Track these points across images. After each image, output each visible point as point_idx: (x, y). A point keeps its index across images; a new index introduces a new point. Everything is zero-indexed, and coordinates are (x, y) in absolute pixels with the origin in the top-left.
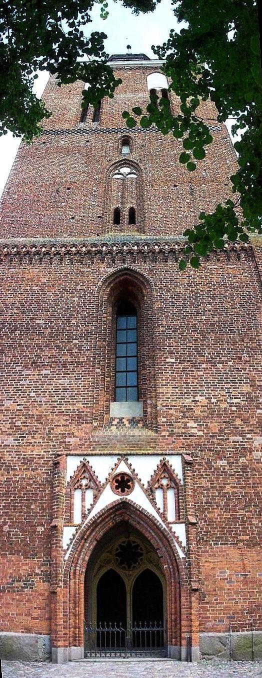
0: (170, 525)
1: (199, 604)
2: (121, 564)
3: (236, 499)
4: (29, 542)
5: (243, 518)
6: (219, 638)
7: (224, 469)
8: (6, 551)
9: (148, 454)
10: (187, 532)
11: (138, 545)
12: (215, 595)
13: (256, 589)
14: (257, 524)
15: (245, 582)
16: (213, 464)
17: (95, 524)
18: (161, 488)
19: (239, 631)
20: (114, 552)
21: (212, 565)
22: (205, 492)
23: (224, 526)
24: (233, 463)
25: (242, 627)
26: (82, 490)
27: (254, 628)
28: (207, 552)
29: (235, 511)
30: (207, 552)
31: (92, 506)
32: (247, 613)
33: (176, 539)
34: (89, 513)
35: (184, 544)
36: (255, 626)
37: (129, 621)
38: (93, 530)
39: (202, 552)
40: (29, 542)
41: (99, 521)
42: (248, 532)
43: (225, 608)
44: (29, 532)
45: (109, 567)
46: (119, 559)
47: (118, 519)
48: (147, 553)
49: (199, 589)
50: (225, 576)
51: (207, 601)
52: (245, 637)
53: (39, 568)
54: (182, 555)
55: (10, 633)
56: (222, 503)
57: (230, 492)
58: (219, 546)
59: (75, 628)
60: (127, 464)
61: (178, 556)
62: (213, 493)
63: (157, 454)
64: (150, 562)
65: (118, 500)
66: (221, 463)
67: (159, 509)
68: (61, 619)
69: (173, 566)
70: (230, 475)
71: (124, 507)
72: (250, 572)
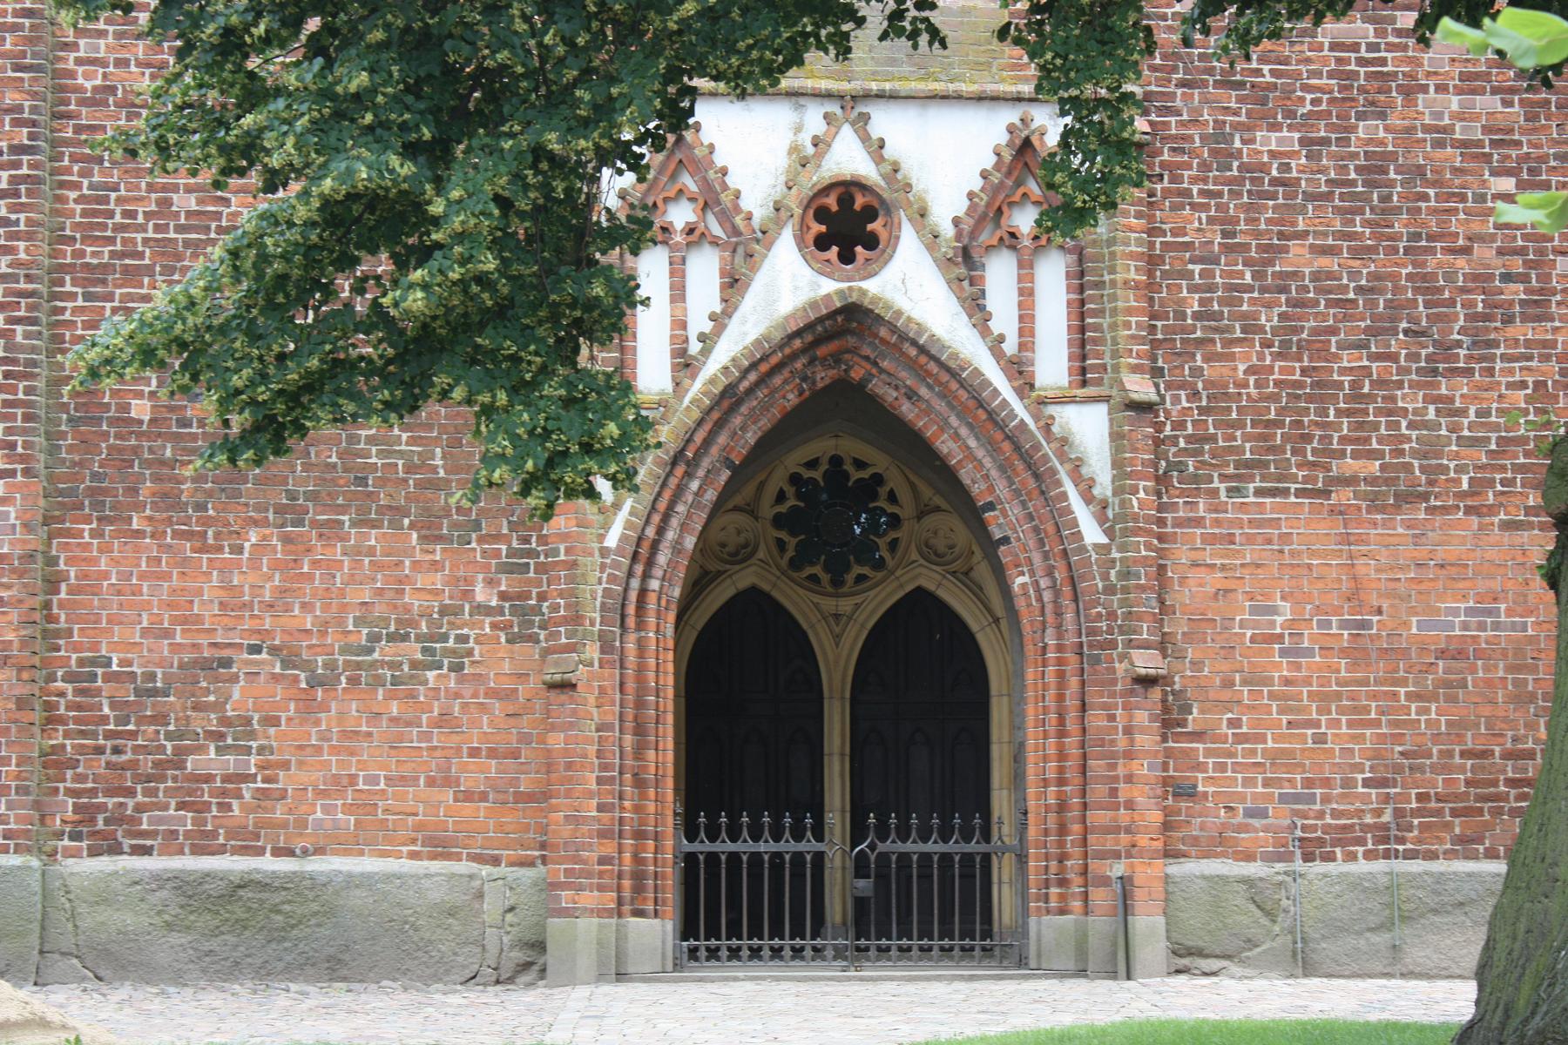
0: (1052, 410)
1: (1164, 739)
2: (795, 564)
3: (1330, 304)
4: (442, 473)
5: (1355, 385)
6: (1248, 882)
7: (1285, 168)
8: (343, 510)
9: (959, 97)
10: (1116, 437)
11: (878, 479)
12: (1227, 705)
13: (1403, 682)
14: (1416, 412)
15: (1356, 654)
16: (1237, 144)
17: (728, 399)
18: (1013, 248)
19: (1334, 860)
20: (768, 510)
21: (1214, 580)
22: (1197, 268)
23: (1272, 416)
24: (1325, 142)
25: (1345, 839)
26: (673, 249)
27: (1401, 848)
28: (1198, 522)
29: (1322, 352)
30: (1198, 522)
31: (720, 321)
32: (1367, 783)
33: (1069, 466)
34: (706, 352)
35: (1104, 483)
36: (1402, 841)
37: (836, 817)
38: (720, 424)
39: (1179, 523)
40: (442, 473)
41: (745, 384)
42: (1375, 445)
43: (1273, 755)
44: (443, 429)
45: (745, 578)
46: (792, 542)
47: (823, 377)
48: (920, 516)
49: (1164, 677)
50: (1272, 624)
51: (1198, 729)
52: (1357, 884)
53: (490, 582)
54: (1092, 533)
55: (357, 860)
56: (1268, 320)
57: (1307, 271)
58: (1252, 499)
59: (639, 835)
60: (865, 138)
61: (1078, 536)
62: (1231, 274)
63: (995, 99)
64: (933, 555)
65: (828, 296)
66: (1267, 141)
67: (1001, 339)
68: (590, 794)
69: (1054, 580)
70: (1310, 197)
71: (845, 327)
72: (1379, 612)
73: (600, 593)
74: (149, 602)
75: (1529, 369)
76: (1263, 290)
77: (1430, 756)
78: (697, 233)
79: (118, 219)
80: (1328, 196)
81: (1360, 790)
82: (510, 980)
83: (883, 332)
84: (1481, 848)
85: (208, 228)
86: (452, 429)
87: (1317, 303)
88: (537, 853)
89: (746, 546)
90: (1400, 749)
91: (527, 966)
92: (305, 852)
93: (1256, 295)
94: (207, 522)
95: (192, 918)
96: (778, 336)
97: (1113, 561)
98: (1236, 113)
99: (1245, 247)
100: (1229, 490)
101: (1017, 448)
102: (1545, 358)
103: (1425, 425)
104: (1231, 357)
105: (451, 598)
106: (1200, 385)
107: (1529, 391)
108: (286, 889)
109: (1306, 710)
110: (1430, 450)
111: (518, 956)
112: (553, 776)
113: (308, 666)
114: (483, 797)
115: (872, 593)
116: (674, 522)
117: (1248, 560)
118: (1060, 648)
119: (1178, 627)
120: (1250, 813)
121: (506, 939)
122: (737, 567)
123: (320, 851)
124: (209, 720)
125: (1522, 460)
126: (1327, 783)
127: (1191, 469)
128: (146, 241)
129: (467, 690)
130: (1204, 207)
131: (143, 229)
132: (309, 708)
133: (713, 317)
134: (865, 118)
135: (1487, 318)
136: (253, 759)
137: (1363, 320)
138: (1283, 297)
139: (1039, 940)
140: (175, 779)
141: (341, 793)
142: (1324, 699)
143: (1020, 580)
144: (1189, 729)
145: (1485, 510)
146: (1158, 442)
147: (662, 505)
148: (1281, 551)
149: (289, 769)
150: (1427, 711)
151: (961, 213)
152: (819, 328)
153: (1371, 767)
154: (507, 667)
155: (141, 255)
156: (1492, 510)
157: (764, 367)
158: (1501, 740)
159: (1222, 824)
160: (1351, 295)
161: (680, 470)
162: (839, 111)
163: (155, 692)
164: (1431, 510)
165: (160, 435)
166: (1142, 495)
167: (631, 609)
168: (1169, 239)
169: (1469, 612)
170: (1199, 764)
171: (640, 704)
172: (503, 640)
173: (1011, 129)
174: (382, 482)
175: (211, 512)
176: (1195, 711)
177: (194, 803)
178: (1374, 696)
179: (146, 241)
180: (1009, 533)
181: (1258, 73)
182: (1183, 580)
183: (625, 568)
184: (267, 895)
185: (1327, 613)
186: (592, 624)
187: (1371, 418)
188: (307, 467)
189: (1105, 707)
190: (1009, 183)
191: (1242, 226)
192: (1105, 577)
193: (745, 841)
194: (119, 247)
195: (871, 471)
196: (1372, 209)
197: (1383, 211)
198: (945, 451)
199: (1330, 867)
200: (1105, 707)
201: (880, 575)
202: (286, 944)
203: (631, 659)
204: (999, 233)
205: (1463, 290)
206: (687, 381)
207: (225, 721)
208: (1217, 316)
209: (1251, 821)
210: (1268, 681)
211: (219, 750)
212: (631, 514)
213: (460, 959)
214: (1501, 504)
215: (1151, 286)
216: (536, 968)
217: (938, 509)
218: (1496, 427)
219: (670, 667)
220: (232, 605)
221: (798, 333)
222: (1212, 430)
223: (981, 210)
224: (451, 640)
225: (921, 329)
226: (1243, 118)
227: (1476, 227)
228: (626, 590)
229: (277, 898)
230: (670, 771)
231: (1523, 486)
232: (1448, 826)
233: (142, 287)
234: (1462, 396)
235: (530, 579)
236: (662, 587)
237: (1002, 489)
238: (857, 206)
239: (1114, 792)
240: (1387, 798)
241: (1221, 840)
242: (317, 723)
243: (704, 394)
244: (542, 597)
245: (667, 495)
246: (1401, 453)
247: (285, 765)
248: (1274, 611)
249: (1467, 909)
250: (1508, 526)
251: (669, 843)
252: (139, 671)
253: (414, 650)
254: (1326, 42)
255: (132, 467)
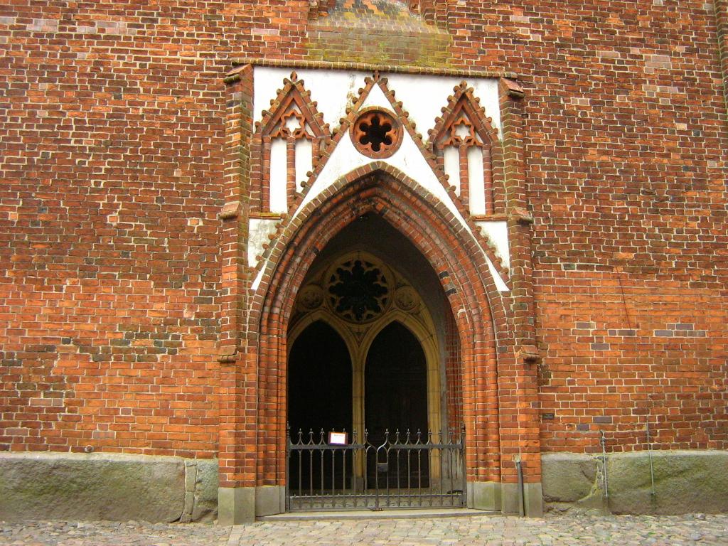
0: (479, 224)
2: (340, 310)
4: (168, 251)
5: (622, 217)
6: (581, 464)
8: (114, 269)
14: (650, 230)
16: (562, 102)
17: (316, 215)
19: (621, 451)
20: (327, 285)
27: (652, 444)
28: (551, 282)
29: (606, 200)
30: (551, 282)
31: (312, 176)
32: (635, 412)
34: (306, 191)
35: (506, 263)
36: (652, 440)
38: (310, 230)
39: (541, 282)
40: (168, 251)
43: (590, 398)
47: (363, 208)
48: (397, 288)
52: (633, 462)
53: (191, 308)
54: (501, 286)
55: (117, 454)
56: (581, 185)
58: (576, 270)
60: (385, 89)
61: (494, 287)
62: (562, 162)
64: (403, 306)
65: (367, 165)
66: (577, 101)
67: (454, 188)
72: (638, 327)
73: (249, 313)
74: (12, 316)
75: (698, 211)
76: (577, 170)
77: (664, 398)
78: (301, 134)
79: (8, 121)
80: (604, 128)
81: (632, 415)
82: (199, 520)
83: (395, 185)
84: (689, 443)
85: (54, 126)
86: (173, 229)
87: (602, 177)
88: (214, 451)
89: (317, 300)
90: (650, 394)
91: (207, 512)
92: (90, 451)
93: (574, 172)
94: (44, 274)
95: (28, 485)
96: (342, 185)
97: (512, 300)
98: (561, 88)
99: (567, 150)
100: (565, 266)
101: (462, 242)
102: (705, 207)
103: (654, 236)
104: (564, 201)
105: (170, 316)
106: (549, 214)
107: (699, 222)
108: (78, 470)
109: (604, 375)
110: (657, 248)
111: (202, 507)
112: (223, 410)
113: (94, 351)
114: (186, 421)
115: (375, 323)
116: (287, 278)
117: (575, 301)
118: (483, 345)
119: (543, 334)
120: (580, 428)
121: (196, 498)
122: (314, 310)
123: (97, 449)
124: (41, 379)
125: (698, 254)
126: (616, 412)
127: (547, 255)
128: (21, 133)
129: (178, 365)
130: (548, 131)
131: (21, 126)
132: (94, 373)
133: (309, 175)
134: (385, 82)
135: (678, 187)
136: (63, 400)
137: (624, 186)
138: (586, 174)
139: (473, 494)
140: (22, 410)
141: (110, 418)
142: (615, 371)
143: (461, 311)
144: (550, 385)
145: (683, 277)
146: (532, 242)
147: (281, 269)
148: (591, 296)
149: (82, 406)
150: (662, 376)
151: (432, 128)
152: (362, 182)
153: (637, 404)
154: (199, 352)
155: (18, 139)
156: (686, 278)
157: (334, 201)
158: (696, 390)
159: (568, 433)
160: (618, 174)
161: (291, 251)
162: (372, 79)
163: (13, 363)
164: (659, 277)
165: (22, 229)
166: (525, 266)
167: (265, 323)
168: (532, 144)
169: (678, 327)
170: (555, 403)
171: (268, 373)
172: (197, 338)
173: (455, 90)
174: (136, 255)
175: (47, 269)
176: (552, 376)
177: (31, 422)
178: (637, 368)
179: (21, 133)
180: (455, 287)
181: (570, 70)
182: (544, 310)
183: (262, 301)
184: (69, 473)
185: (613, 327)
186: (245, 330)
187: (630, 232)
188: (98, 247)
189: (509, 374)
190: (456, 115)
191: (566, 140)
192: (508, 308)
193: (300, 444)
194: (8, 135)
195: (374, 267)
196: (625, 135)
197: (630, 136)
198: (423, 246)
199: (619, 455)
200: (509, 374)
201: (379, 314)
202: (79, 500)
203: (264, 349)
204: (450, 140)
205: (668, 174)
206: (295, 206)
207: (50, 379)
208: (556, 182)
209: (580, 432)
210: (587, 361)
211: (45, 395)
212: (265, 273)
213: (172, 509)
214: (690, 275)
215: (524, 167)
216: (213, 513)
217: (404, 285)
218: (686, 238)
219: (285, 354)
220: (56, 318)
221: (352, 184)
222: (556, 237)
223: (441, 126)
224: (170, 338)
225: (414, 183)
226: (564, 90)
227: (671, 144)
228: (262, 313)
229: (73, 475)
230: (284, 407)
231: (699, 266)
232: (673, 433)
233: (18, 155)
234: (670, 223)
235: (212, 307)
236: (281, 312)
237: (452, 265)
238: (381, 123)
239: (515, 418)
240: (645, 419)
241: (567, 442)
242: (98, 380)
243: (304, 212)
244: (218, 316)
245: (284, 263)
246: (644, 249)
247: (81, 403)
248: (589, 326)
249: (684, 474)
250: (694, 285)
251: (283, 446)
252: (5, 352)
253: (150, 342)
254: (600, 58)
255: (7, 245)
